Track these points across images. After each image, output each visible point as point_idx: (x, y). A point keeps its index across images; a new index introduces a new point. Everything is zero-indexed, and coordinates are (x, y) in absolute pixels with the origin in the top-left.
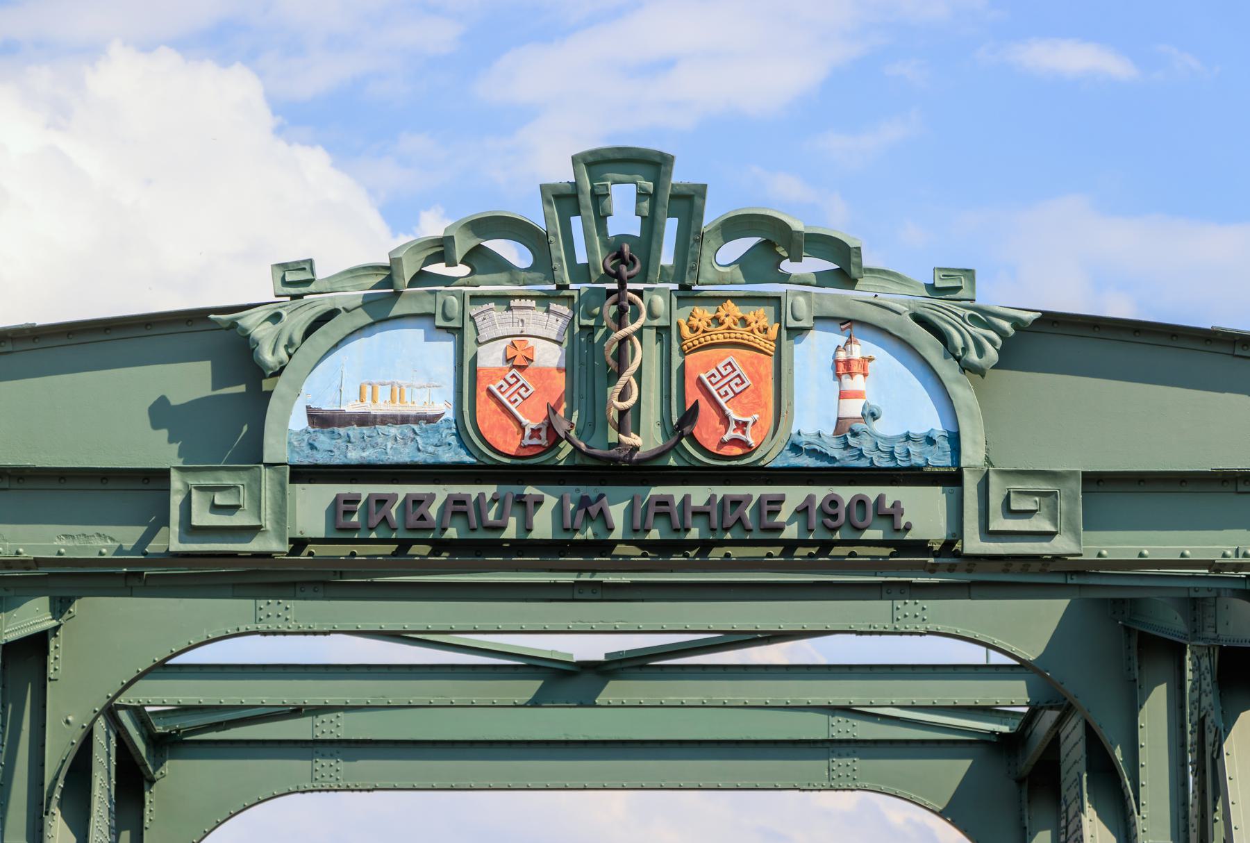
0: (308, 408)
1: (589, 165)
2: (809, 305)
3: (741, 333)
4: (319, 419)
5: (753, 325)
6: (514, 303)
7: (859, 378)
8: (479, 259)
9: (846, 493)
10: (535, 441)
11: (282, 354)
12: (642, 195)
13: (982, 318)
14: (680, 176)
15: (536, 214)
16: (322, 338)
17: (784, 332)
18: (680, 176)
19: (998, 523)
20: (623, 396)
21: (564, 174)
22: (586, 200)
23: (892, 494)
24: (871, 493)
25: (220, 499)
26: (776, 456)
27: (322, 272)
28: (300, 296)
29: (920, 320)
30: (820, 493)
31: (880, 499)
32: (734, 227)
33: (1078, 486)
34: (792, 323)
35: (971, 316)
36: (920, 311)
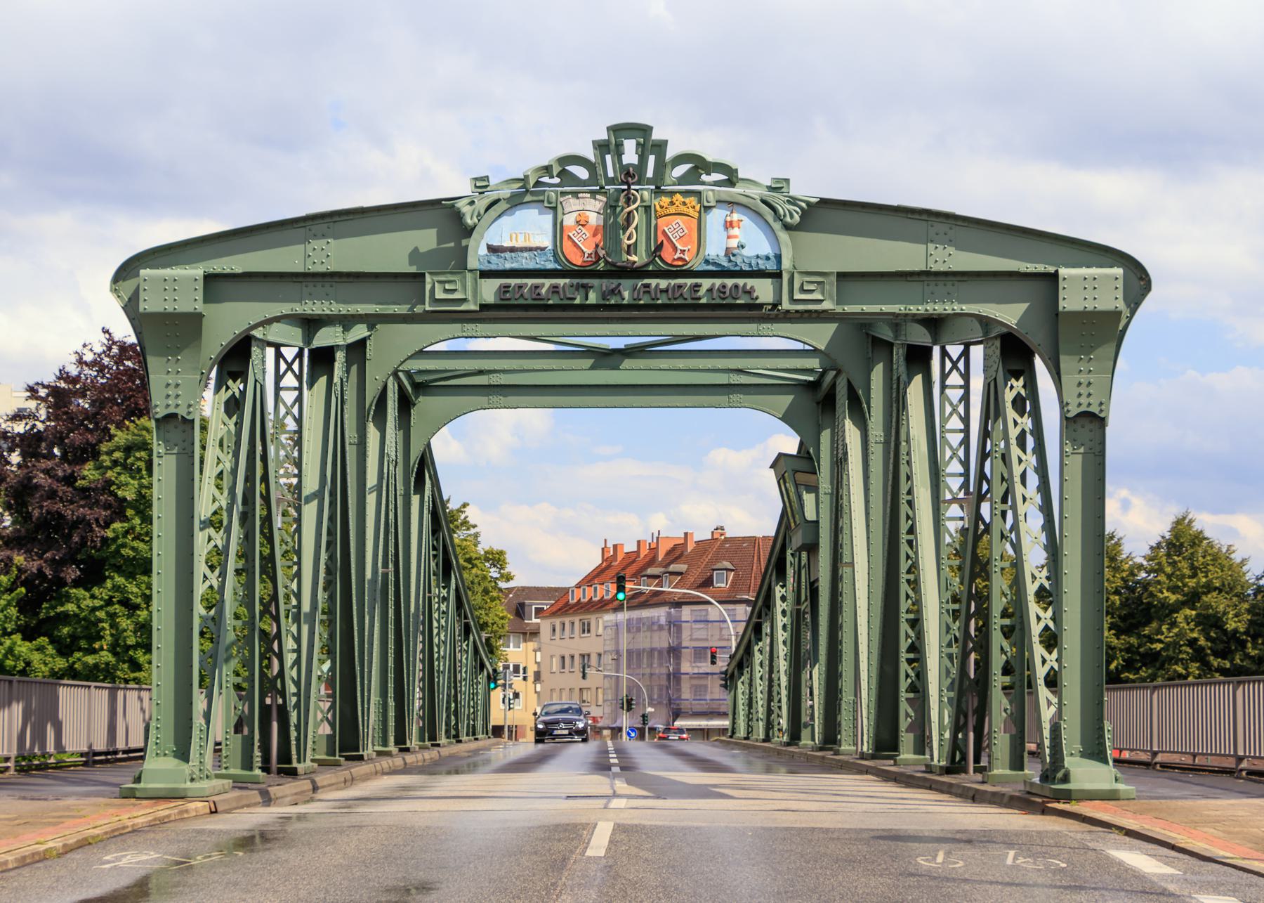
0: (487, 244)
1: (614, 131)
2: (714, 194)
3: (683, 209)
4: (492, 249)
5: (689, 205)
6: (580, 195)
7: (736, 229)
8: (563, 173)
9: (730, 282)
10: (590, 259)
11: (476, 220)
12: (638, 144)
13: (793, 201)
14: (656, 135)
15: (590, 154)
16: (493, 212)
17: (702, 209)
18: (656, 135)
19: (798, 296)
20: (629, 239)
21: (603, 135)
22: (612, 147)
23: (750, 282)
24: (741, 282)
25: (448, 286)
26: (698, 266)
27: (493, 181)
28: (483, 193)
29: (764, 202)
30: (718, 282)
31: (745, 285)
32: (681, 159)
33: (834, 278)
34: (706, 204)
35: (788, 201)
36: (764, 198)
